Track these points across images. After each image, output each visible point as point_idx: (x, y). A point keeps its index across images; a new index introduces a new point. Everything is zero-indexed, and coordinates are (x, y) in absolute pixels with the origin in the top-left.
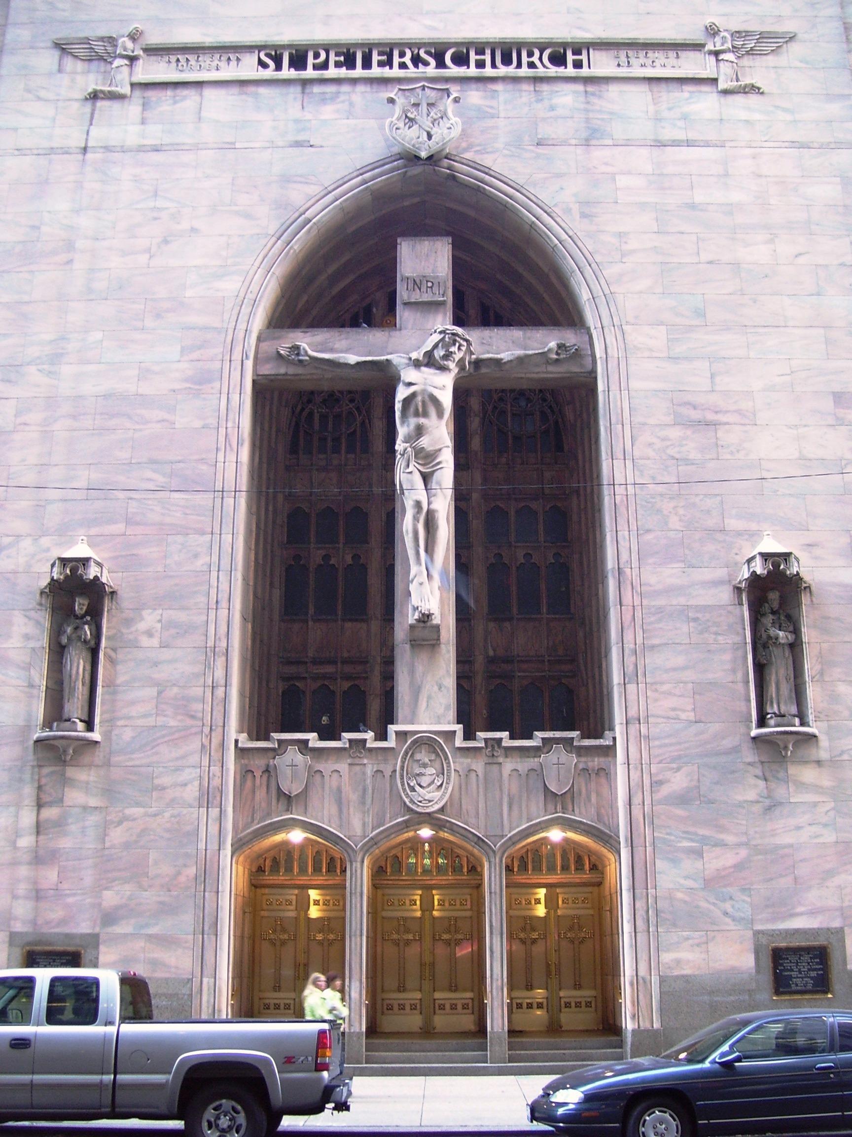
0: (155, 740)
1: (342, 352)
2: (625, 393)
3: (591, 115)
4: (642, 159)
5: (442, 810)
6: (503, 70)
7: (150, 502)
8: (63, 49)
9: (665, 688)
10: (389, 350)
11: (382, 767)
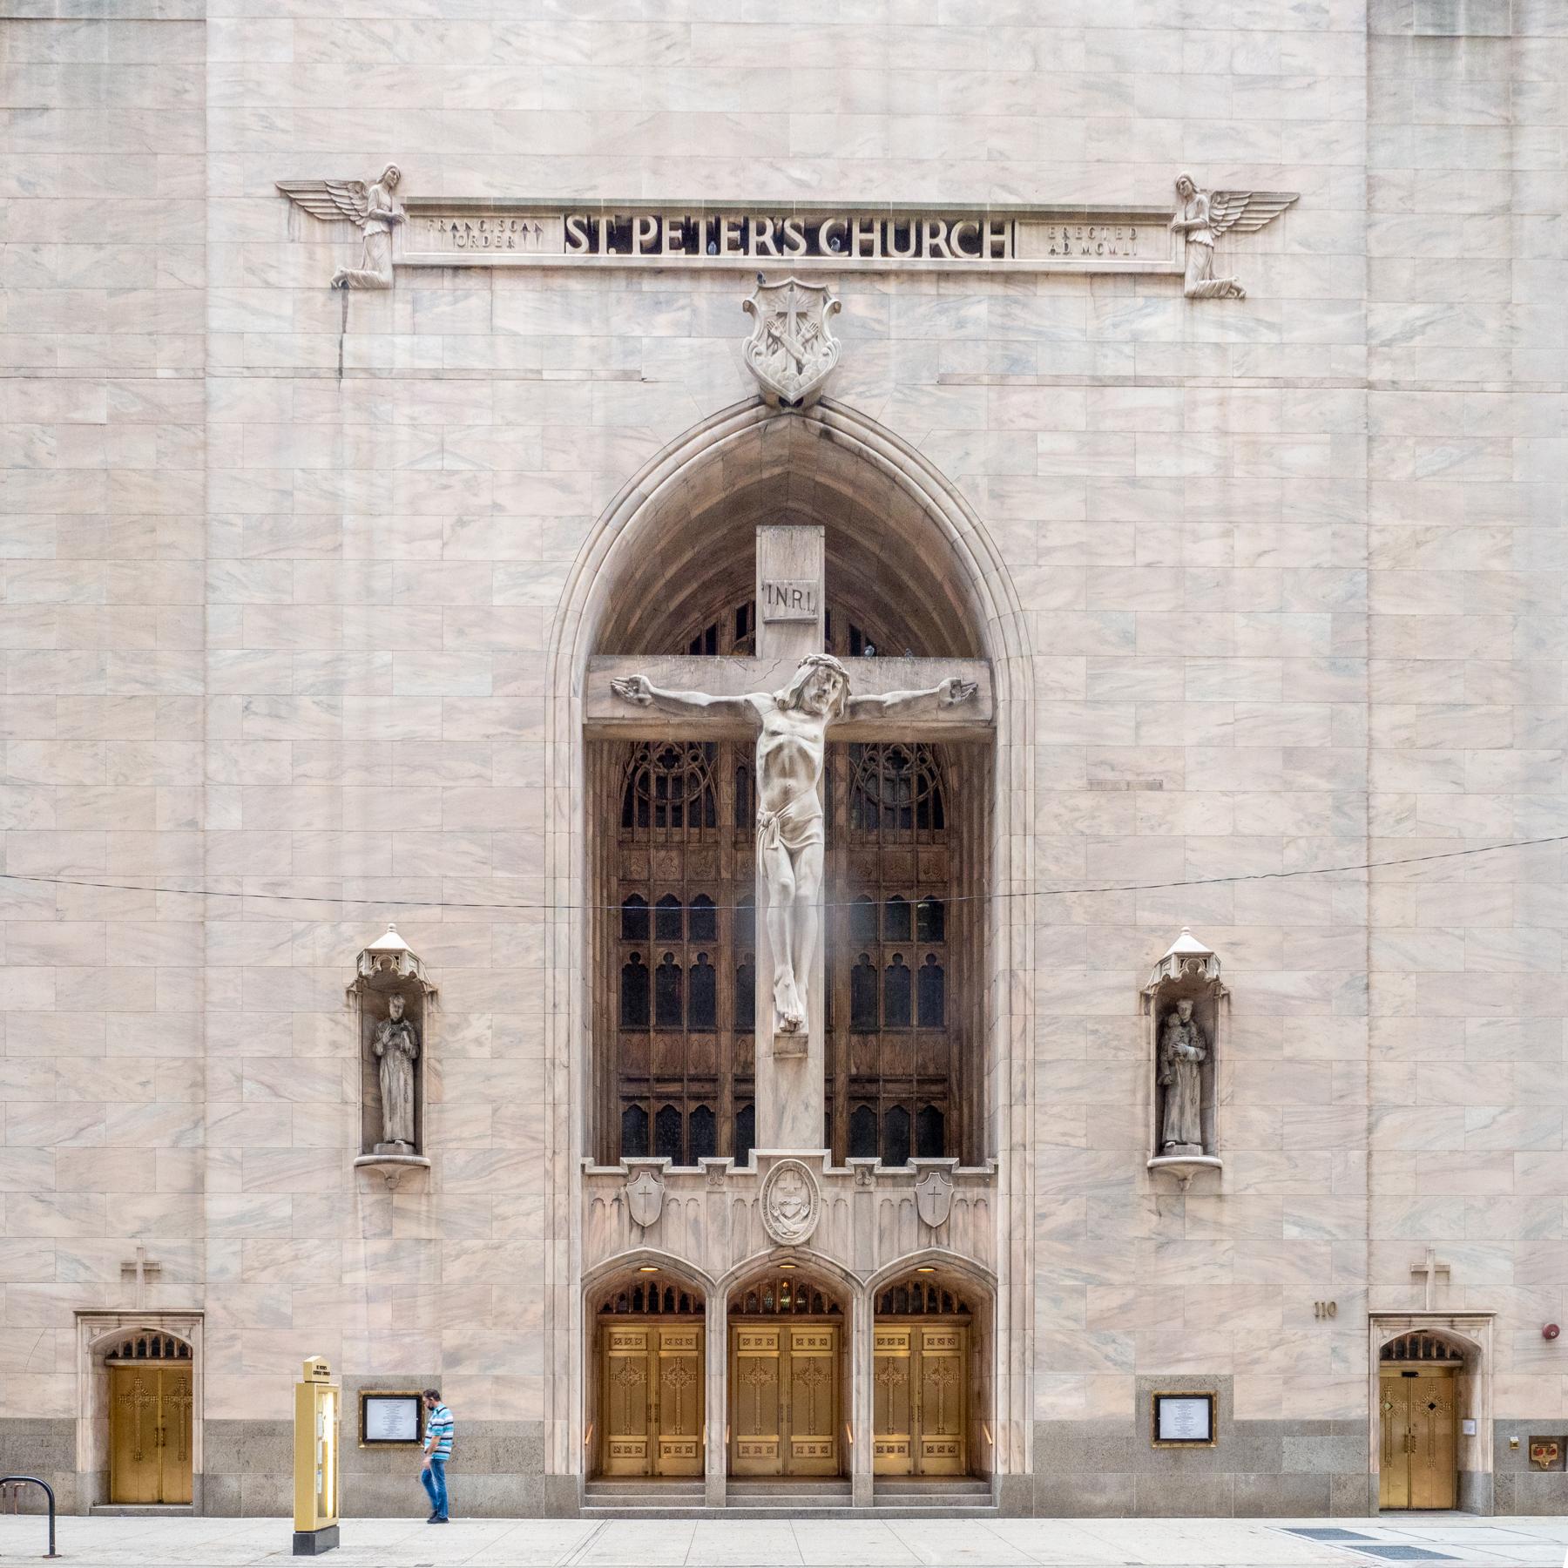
0: (492, 1164)
1: (690, 688)
2: (1030, 748)
3: (1012, 336)
4: (1072, 406)
5: (808, 1242)
6: (898, 260)
7: (468, 882)
8: (292, 200)
9: (1055, 1110)
10: (747, 688)
11: (744, 1195)
